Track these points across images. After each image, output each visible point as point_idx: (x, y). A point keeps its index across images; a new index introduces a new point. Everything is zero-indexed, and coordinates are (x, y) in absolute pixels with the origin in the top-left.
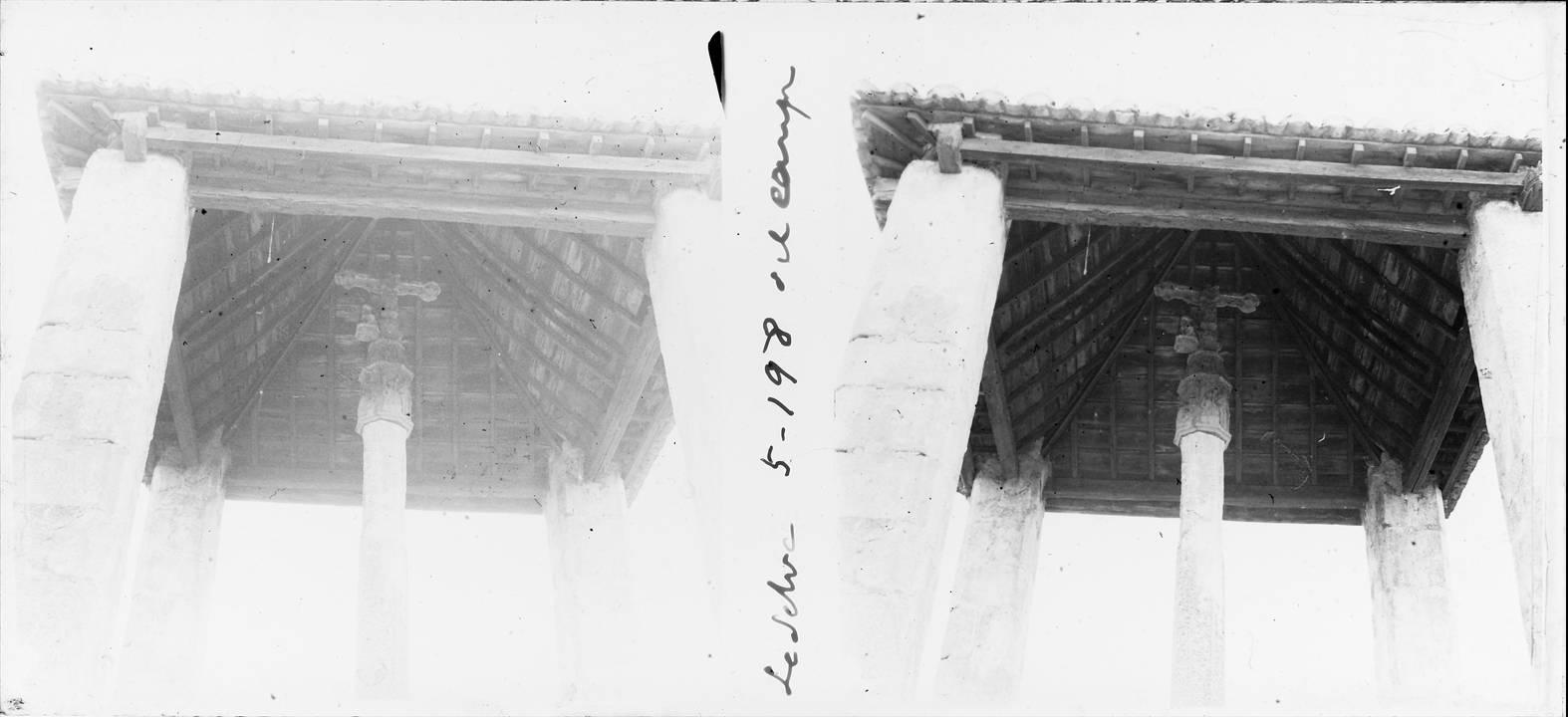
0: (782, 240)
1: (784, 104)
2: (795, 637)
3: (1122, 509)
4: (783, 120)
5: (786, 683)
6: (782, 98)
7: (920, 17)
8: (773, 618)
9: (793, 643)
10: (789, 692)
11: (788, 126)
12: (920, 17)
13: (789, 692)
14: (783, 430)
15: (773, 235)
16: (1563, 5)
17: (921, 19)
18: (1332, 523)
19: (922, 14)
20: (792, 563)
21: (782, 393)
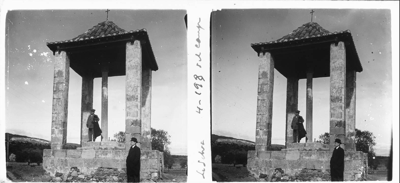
0: (199, 56)
1: (199, 27)
2: (200, 60)
3: (353, 97)
4: (198, 30)
5: (203, 175)
6: (203, 154)
7: (235, 4)
8: (197, 171)
9: (201, 68)
10: (204, 178)
11: (200, 35)
12: (235, 4)
13: (204, 178)
14: (200, 100)
15: (196, 55)
16: (399, 1)
17: (235, 5)
18: (391, 26)
19: (235, 4)
20: (201, 57)
21: (203, 146)
